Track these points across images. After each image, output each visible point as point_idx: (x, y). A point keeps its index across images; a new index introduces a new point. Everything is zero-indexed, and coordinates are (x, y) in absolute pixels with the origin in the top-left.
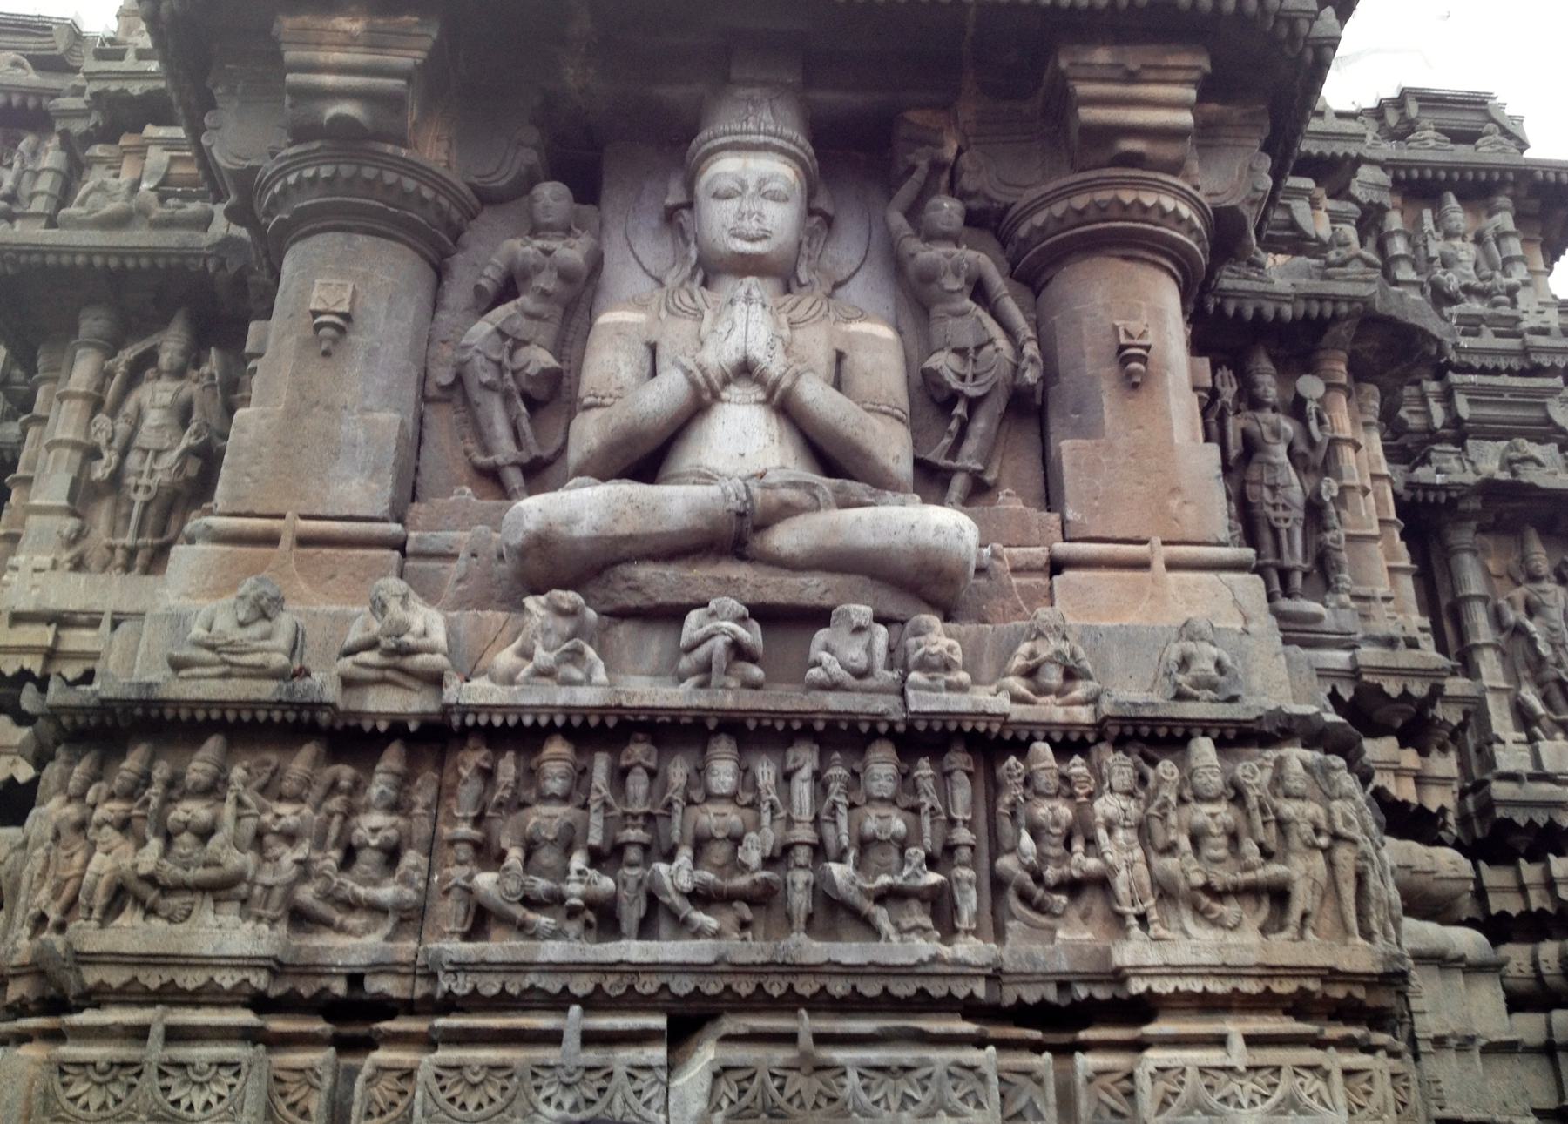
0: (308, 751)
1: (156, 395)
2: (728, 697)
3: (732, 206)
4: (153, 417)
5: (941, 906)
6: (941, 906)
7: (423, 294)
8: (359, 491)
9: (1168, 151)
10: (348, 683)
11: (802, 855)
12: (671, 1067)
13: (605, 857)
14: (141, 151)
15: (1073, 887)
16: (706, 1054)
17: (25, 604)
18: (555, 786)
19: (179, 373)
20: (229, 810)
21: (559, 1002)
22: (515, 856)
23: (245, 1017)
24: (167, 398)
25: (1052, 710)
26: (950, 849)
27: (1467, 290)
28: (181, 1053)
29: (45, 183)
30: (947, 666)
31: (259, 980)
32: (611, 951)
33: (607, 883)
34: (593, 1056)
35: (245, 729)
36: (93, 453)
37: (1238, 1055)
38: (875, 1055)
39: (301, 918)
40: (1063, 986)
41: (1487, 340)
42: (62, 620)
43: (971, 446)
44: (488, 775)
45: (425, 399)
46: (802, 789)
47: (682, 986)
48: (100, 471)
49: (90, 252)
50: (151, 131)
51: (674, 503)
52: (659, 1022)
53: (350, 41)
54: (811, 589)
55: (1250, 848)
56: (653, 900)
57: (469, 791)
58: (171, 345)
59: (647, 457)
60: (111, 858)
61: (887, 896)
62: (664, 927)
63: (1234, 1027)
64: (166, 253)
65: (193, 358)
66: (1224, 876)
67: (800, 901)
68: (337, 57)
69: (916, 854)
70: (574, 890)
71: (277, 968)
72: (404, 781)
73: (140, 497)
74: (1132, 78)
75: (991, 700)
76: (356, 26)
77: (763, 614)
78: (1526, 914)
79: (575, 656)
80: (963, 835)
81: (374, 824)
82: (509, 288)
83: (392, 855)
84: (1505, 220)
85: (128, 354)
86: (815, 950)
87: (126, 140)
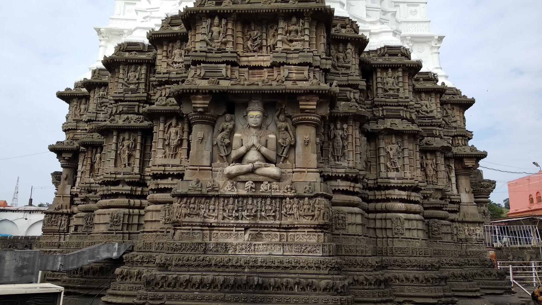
0: (204, 199)
1: (173, 130)
2: (250, 193)
3: (252, 119)
4: (173, 135)
5: (274, 217)
6: (274, 217)
7: (212, 131)
8: (206, 162)
9: (313, 111)
10: (208, 191)
11: (259, 211)
12: (245, 234)
13: (237, 211)
14: (165, 89)
15: (290, 215)
16: (248, 232)
17: (160, 164)
18: (231, 203)
19: (175, 127)
20: (196, 206)
21: (233, 227)
22: (227, 211)
23: (200, 228)
24: (174, 131)
25: (289, 194)
26: (276, 210)
27: (390, 89)
28: (194, 231)
29: (143, 76)
30: (277, 189)
31: (201, 224)
32: (238, 222)
33: (237, 214)
34: (236, 233)
35: (196, 196)
36: (165, 140)
37: (306, 233)
38: (266, 233)
39: (205, 217)
40: (288, 225)
41: (391, 100)
42: (164, 166)
43: (284, 153)
44: (224, 201)
45: (213, 146)
46: (259, 204)
47: (246, 225)
48: (166, 143)
49: (161, 110)
50: (166, 86)
51: (246, 167)
52: (243, 229)
53: (200, 99)
54: (260, 178)
55: (310, 211)
56: (242, 216)
57: (222, 204)
58: (174, 122)
59: (240, 159)
60: (184, 211)
61: (268, 216)
62: (244, 219)
63: (306, 230)
64: (172, 110)
65: (177, 124)
66: (306, 214)
67: (259, 216)
68: (199, 102)
69: (272, 211)
70: (234, 215)
71: (203, 223)
72: (215, 202)
73: (172, 147)
74: (308, 101)
75: (281, 193)
76: (201, 97)
77: (254, 182)
78: (381, 199)
79: (233, 188)
80: (278, 209)
81: (212, 207)
82: (223, 130)
83: (214, 210)
84: (400, 74)
85: (168, 124)
86: (260, 222)
87: (163, 87)
